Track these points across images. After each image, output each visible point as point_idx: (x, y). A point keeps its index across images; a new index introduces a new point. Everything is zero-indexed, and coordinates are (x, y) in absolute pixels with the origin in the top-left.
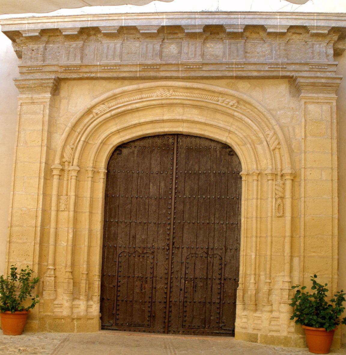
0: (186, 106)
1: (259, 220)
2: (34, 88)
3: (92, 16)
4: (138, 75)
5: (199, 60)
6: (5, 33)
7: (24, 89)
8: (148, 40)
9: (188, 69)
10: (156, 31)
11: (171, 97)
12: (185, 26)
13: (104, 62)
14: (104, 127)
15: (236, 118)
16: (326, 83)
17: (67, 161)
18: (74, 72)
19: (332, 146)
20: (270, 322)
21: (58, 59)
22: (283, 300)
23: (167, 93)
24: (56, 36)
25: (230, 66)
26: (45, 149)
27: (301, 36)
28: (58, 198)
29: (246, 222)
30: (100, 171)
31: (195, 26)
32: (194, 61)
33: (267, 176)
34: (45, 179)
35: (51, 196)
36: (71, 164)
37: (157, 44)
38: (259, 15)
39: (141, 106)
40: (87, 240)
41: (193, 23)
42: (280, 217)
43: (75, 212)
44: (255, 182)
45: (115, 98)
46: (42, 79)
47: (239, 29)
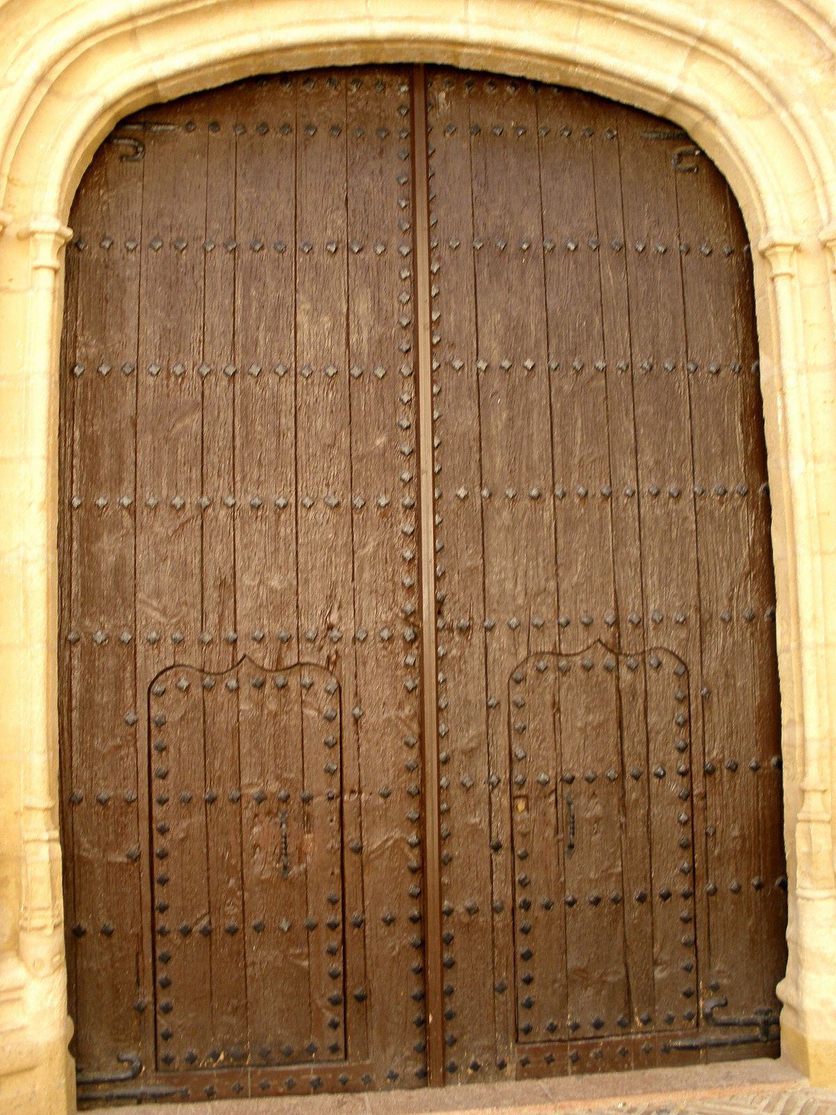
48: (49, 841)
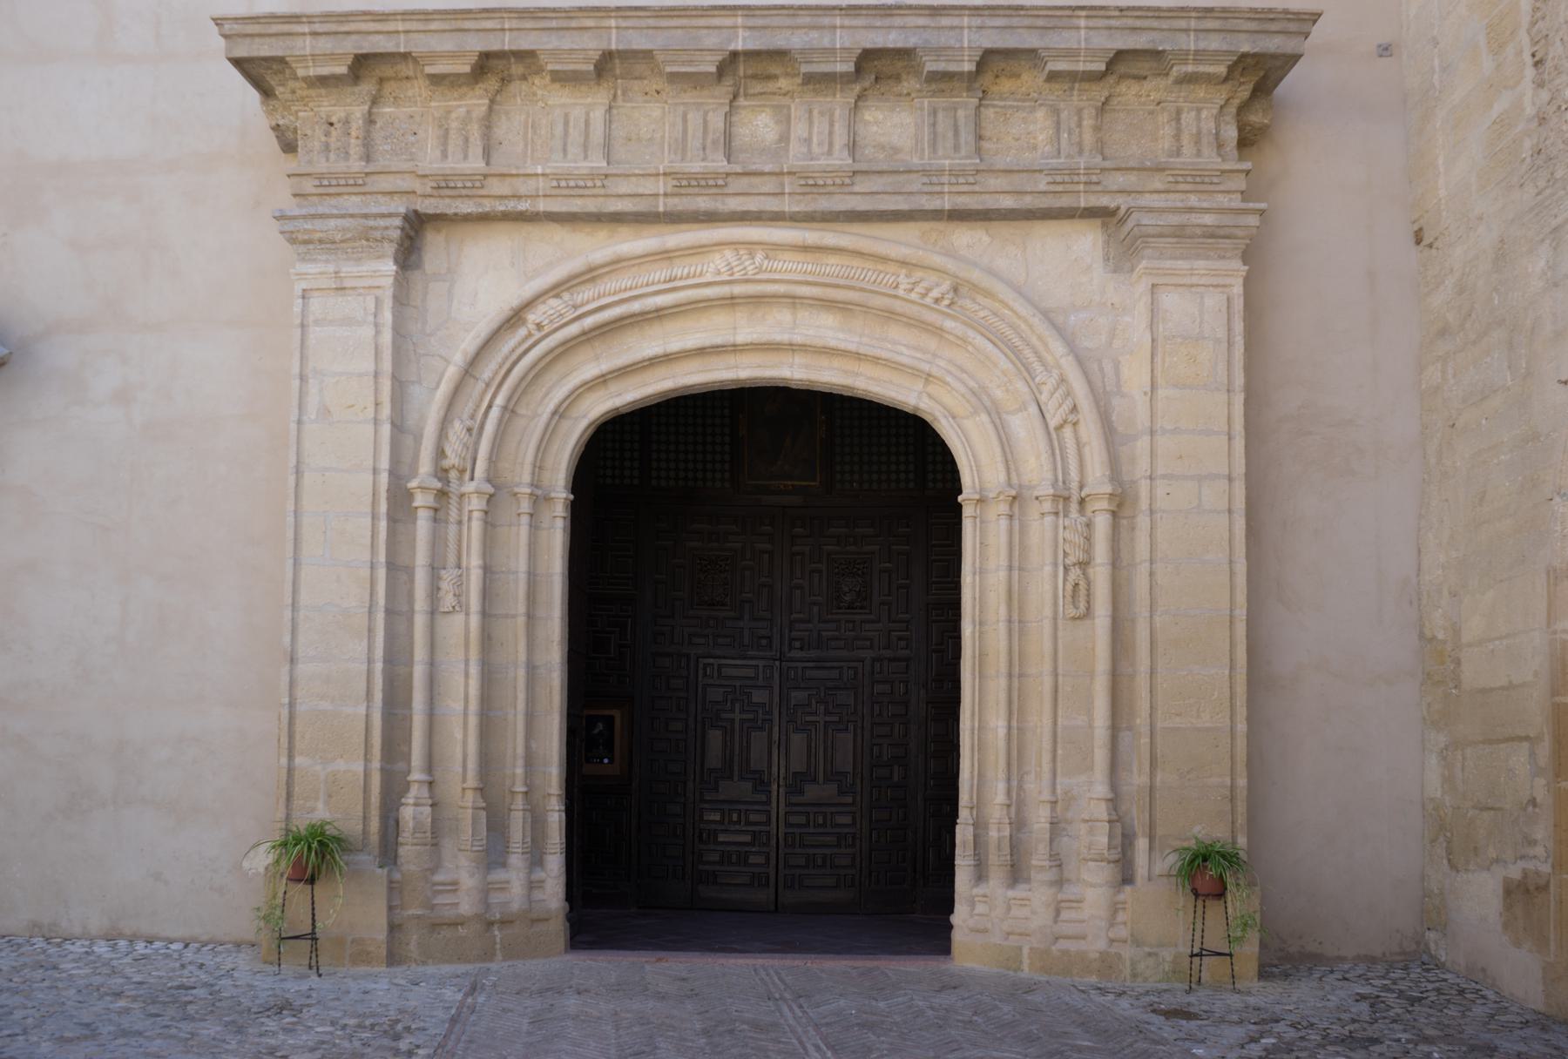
0: (802, 304)
1: (1017, 629)
2: (342, 245)
3: (516, 15)
4: (661, 209)
5: (841, 159)
6: (238, 63)
7: (311, 247)
8: (689, 97)
9: (808, 189)
10: (713, 69)
11: (758, 277)
12: (802, 51)
13: (557, 164)
14: (560, 367)
15: (947, 336)
16: (1218, 227)
17: (454, 466)
18: (467, 196)
19: (1229, 414)
20: (1058, 912)
21: (411, 153)
22: (1092, 851)
23: (747, 263)
24: (401, 80)
25: (935, 179)
26: (386, 430)
27: (1148, 85)
28: (433, 576)
29: (977, 635)
30: (553, 495)
31: (831, 51)
32: (828, 165)
33: (1040, 502)
34: (392, 520)
35: (410, 571)
36: (467, 476)
37: (714, 110)
38: (1024, 16)
39: (670, 304)
40: (521, 696)
41: (826, 43)
42: (1079, 618)
43: (485, 614)
44: (1004, 523)
45: (593, 279)
46: (366, 216)
47: (963, 61)
48: (559, 811)
